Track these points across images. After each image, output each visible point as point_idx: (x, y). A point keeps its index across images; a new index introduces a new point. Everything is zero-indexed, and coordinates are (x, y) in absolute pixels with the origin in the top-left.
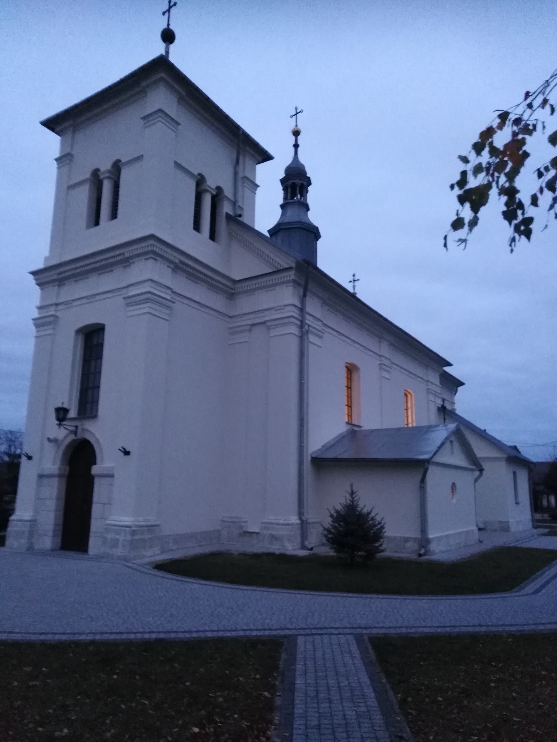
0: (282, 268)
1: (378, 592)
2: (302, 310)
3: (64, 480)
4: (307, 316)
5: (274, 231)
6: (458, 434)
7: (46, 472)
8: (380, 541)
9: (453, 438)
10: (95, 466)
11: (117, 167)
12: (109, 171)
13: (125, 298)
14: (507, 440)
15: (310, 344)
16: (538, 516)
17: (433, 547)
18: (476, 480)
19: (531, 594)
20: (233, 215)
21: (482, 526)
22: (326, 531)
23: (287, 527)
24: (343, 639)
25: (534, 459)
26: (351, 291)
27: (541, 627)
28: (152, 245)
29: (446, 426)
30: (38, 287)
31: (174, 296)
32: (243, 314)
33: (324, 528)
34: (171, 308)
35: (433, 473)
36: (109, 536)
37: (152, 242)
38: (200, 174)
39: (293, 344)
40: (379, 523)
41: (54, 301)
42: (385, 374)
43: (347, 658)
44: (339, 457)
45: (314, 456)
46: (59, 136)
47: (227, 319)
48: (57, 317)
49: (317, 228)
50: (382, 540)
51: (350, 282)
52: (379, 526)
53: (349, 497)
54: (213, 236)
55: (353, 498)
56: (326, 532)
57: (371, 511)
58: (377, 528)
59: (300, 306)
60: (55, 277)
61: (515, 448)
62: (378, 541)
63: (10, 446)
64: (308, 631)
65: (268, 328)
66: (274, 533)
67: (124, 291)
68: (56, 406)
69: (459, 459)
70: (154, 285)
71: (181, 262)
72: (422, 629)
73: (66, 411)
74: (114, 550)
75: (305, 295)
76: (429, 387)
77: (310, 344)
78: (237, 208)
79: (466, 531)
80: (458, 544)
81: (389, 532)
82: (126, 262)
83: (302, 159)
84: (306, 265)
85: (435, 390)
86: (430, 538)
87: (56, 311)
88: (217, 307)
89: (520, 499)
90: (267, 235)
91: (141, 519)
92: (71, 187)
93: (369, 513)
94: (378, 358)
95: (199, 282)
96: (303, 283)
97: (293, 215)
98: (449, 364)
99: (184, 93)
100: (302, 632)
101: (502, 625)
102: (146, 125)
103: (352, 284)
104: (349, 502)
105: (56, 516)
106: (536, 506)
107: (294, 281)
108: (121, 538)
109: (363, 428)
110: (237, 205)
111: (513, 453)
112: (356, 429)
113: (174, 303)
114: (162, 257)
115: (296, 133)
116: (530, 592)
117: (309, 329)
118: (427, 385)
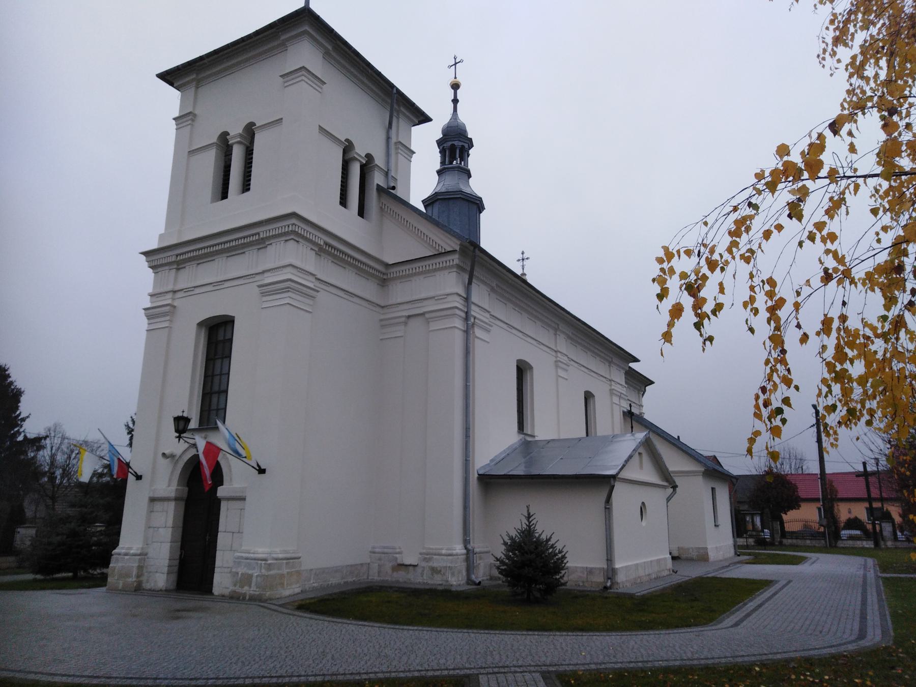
0: (443, 251)
1: (559, 629)
2: (467, 299)
3: (182, 505)
4: (473, 307)
5: (428, 202)
6: (647, 444)
8: (561, 573)
9: (641, 450)
10: (221, 487)
11: (250, 131)
12: (240, 135)
13: (259, 286)
14: (705, 450)
15: (476, 339)
16: (741, 541)
17: (621, 578)
18: (668, 499)
19: (732, 627)
20: (386, 188)
21: (676, 554)
22: (498, 562)
23: (450, 558)
24: (528, 676)
25: (735, 472)
26: (519, 272)
27: (740, 660)
28: (293, 224)
29: (633, 435)
30: (151, 270)
31: (318, 284)
32: (397, 304)
33: (496, 558)
34: (314, 298)
35: (620, 490)
37: (294, 221)
38: (347, 140)
39: (458, 338)
40: (560, 552)
41: (170, 287)
42: (561, 373)
44: (510, 473)
45: (481, 472)
46: (178, 91)
47: (378, 309)
48: (175, 307)
49: (481, 198)
50: (563, 572)
51: (519, 260)
52: (560, 555)
53: (525, 521)
54: (361, 213)
57: (551, 537)
58: (557, 557)
59: (465, 296)
60: (174, 259)
61: (715, 458)
62: (559, 572)
64: (491, 670)
65: (428, 321)
66: (435, 565)
67: (258, 278)
68: (176, 415)
69: (648, 474)
70: (294, 271)
71: (326, 244)
72: (613, 665)
73: (187, 420)
75: (470, 283)
76: (613, 387)
77: (476, 339)
78: (390, 179)
79: (657, 560)
80: (649, 575)
82: (262, 243)
83: (463, 117)
84: (472, 248)
85: (621, 391)
86: (617, 569)
87: (173, 299)
88: (368, 297)
89: (720, 522)
90: (421, 208)
91: (278, 550)
92: (192, 152)
93: (548, 540)
94: (554, 353)
95: (347, 266)
96: (469, 269)
97: (452, 182)
98: (636, 360)
99: (330, 48)
100: (482, 671)
101: (698, 659)
102: (286, 84)
103: (521, 263)
104: (525, 526)
105: (171, 547)
106: (739, 528)
107: (458, 267)
108: (256, 573)
109: (537, 439)
110: (390, 176)
111: (711, 464)
112: (529, 439)
113: (318, 291)
114: (303, 237)
115: (455, 86)
116: (728, 625)
117: (474, 321)
118: (611, 385)
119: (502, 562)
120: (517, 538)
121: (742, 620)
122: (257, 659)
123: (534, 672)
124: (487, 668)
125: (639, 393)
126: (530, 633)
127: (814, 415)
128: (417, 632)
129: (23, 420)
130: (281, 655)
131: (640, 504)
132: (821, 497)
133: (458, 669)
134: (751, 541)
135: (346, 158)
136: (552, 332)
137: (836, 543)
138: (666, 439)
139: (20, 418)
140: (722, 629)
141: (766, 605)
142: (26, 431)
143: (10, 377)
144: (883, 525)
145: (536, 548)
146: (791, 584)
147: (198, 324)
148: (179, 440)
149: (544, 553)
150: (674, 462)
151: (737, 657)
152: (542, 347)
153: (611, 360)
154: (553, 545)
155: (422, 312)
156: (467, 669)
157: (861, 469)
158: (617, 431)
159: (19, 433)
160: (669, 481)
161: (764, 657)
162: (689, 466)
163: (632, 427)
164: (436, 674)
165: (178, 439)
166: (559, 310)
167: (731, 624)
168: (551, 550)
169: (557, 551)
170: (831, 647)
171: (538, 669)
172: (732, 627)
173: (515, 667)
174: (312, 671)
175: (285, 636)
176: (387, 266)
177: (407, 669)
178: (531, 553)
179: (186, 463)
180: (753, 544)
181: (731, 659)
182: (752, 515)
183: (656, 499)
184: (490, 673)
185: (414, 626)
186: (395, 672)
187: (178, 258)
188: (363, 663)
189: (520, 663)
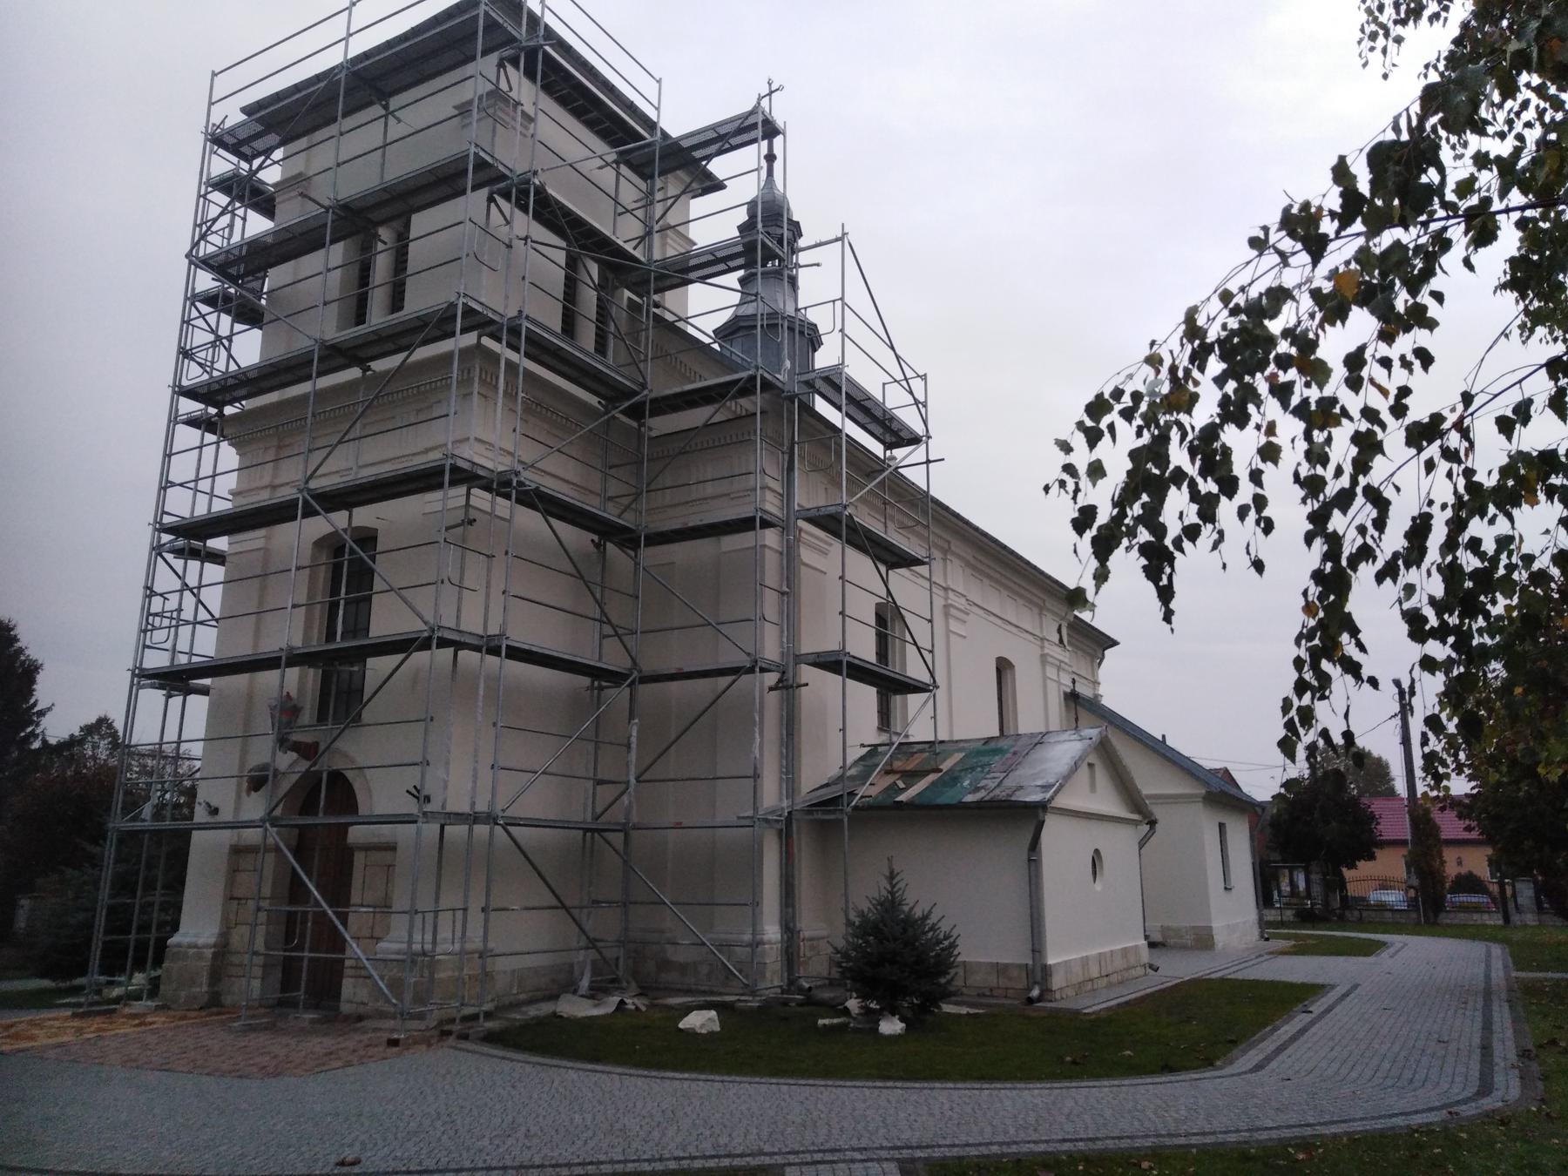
6: (1103, 748)
9: (1092, 759)
14: (1209, 759)
16: (1271, 915)
19: (1252, 1071)
21: (1157, 937)
33: (835, 948)
50: (952, 971)
52: (946, 943)
53: (885, 884)
55: (893, 886)
64: (808, 1158)
69: (1106, 801)
76: (1046, 651)
93: (925, 917)
100: (792, 1158)
104: (884, 893)
121: (1268, 1059)
122: (390, 1136)
123: (887, 1159)
124: (803, 1152)
125: (1092, 662)
126: (890, 1084)
127: (1397, 697)
128: (686, 1084)
129: (42, 713)
130: (435, 1129)
131: (1092, 853)
132: (1409, 838)
133: (749, 1155)
134: (1289, 915)
136: (1036, 611)
137: (1436, 916)
138: (1140, 741)
139: (36, 710)
140: (1233, 1075)
141: (1313, 1030)
142: (47, 733)
143: (18, 640)
144: (1518, 886)
145: (905, 930)
150: (1151, 781)
151: (1258, 1129)
152: (992, 618)
153: (946, 546)
154: (934, 925)
156: (766, 1154)
158: (1055, 725)
159: (34, 735)
160: (1142, 812)
161: (1308, 1131)
162: (1174, 785)
163: (1077, 720)
164: (707, 1165)
166: (960, 524)
167: (1250, 1066)
168: (931, 934)
169: (941, 936)
170: (1431, 1110)
171: (896, 1154)
172: (1252, 1071)
173: (854, 1150)
174: (485, 1161)
177: (657, 1156)
178: (895, 939)
180: (1292, 919)
181: (1247, 1134)
182: (1291, 870)
183: (1120, 844)
184: (807, 1163)
185: (682, 1071)
186: (634, 1161)
188: (579, 1143)
189: (864, 1143)
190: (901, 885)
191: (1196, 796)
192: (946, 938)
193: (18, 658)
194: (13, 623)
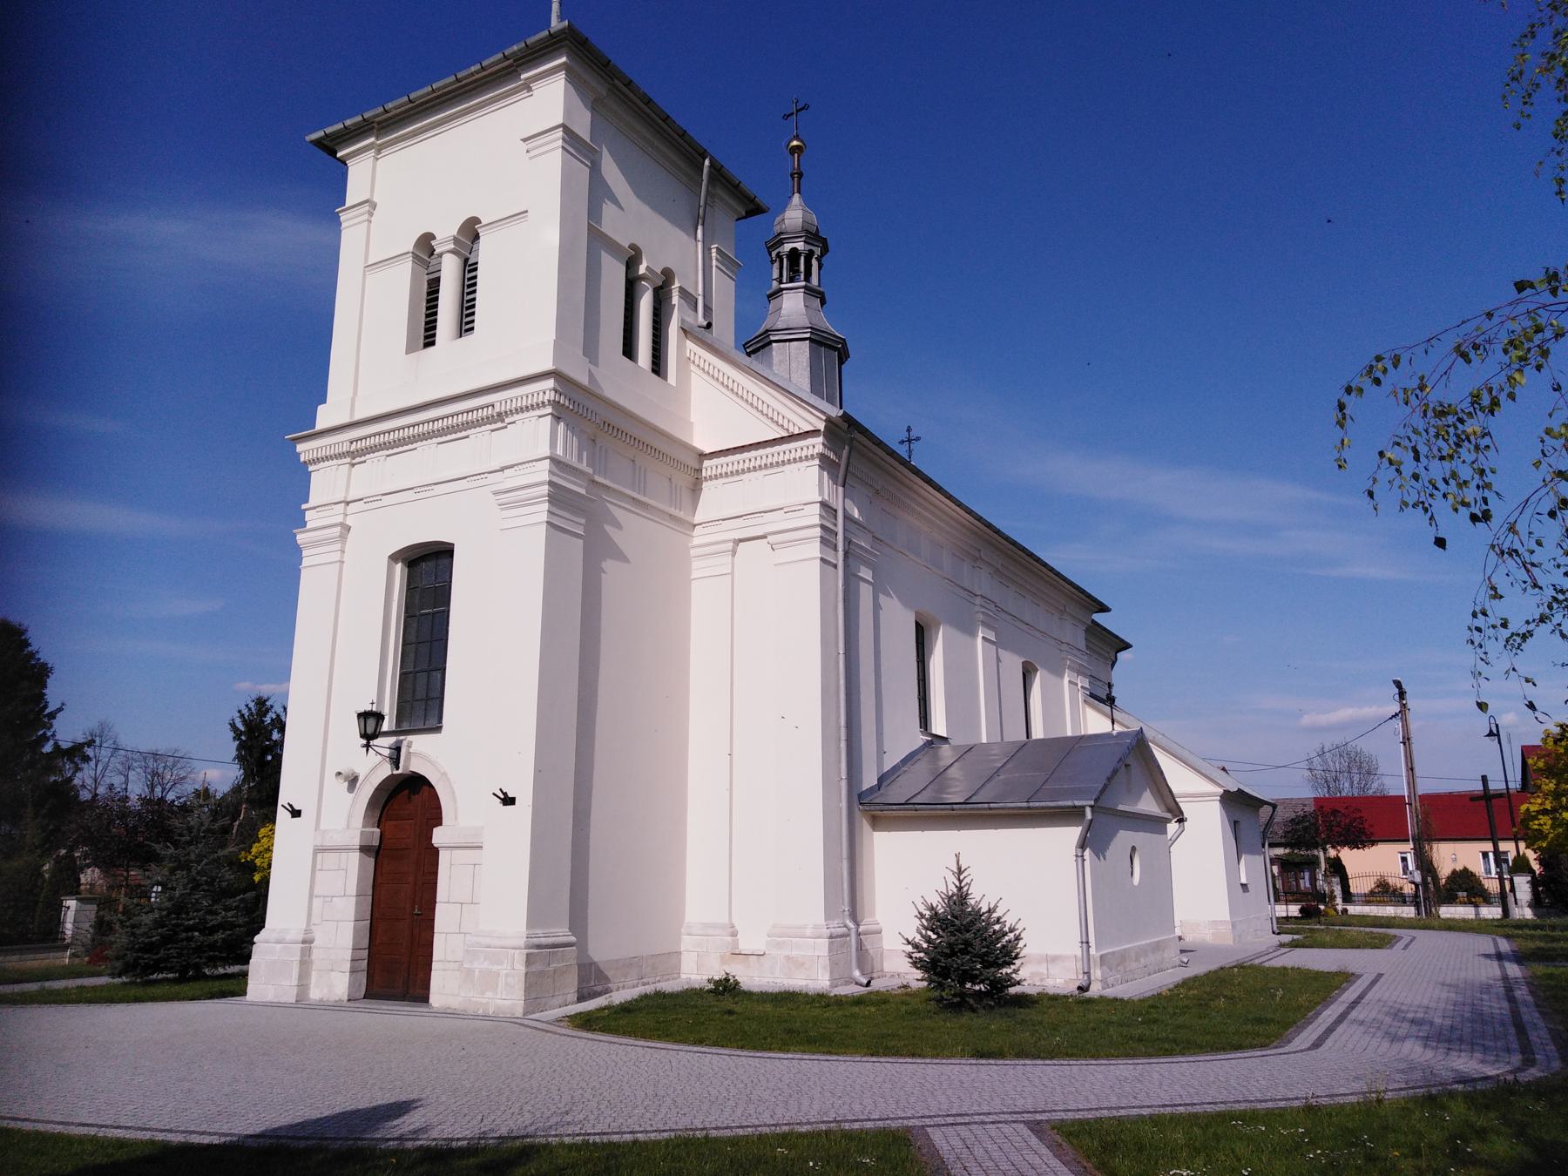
7: (328, 843)
11: (471, 232)
13: (496, 493)
19: (1309, 1049)
33: (907, 940)
36: (480, 965)
38: (633, 247)
43: (1031, 1158)
50: (1018, 962)
51: (918, 439)
52: (1011, 936)
53: (952, 879)
55: (961, 881)
56: (909, 948)
57: (996, 906)
63: (152, 788)
66: (795, 953)
73: (379, 717)
74: (489, 994)
81: (1030, 947)
98: (1104, 609)
105: (355, 928)
107: (822, 457)
119: (917, 946)
120: (940, 907)
127: (1397, 697)
129: (52, 715)
135: (630, 277)
139: (48, 711)
143: (29, 645)
144: (1517, 880)
146: (1382, 979)
147: (390, 557)
148: (367, 750)
149: (986, 929)
154: (999, 919)
155: (761, 534)
157: (1479, 787)
159: (45, 739)
165: (365, 749)
169: (1006, 929)
172: (1309, 1049)
175: (580, 1070)
176: (703, 456)
179: (376, 789)
187: (354, 446)
190: (967, 880)
191: (1210, 795)
192: (1011, 930)
193: (29, 661)
194: (24, 627)
